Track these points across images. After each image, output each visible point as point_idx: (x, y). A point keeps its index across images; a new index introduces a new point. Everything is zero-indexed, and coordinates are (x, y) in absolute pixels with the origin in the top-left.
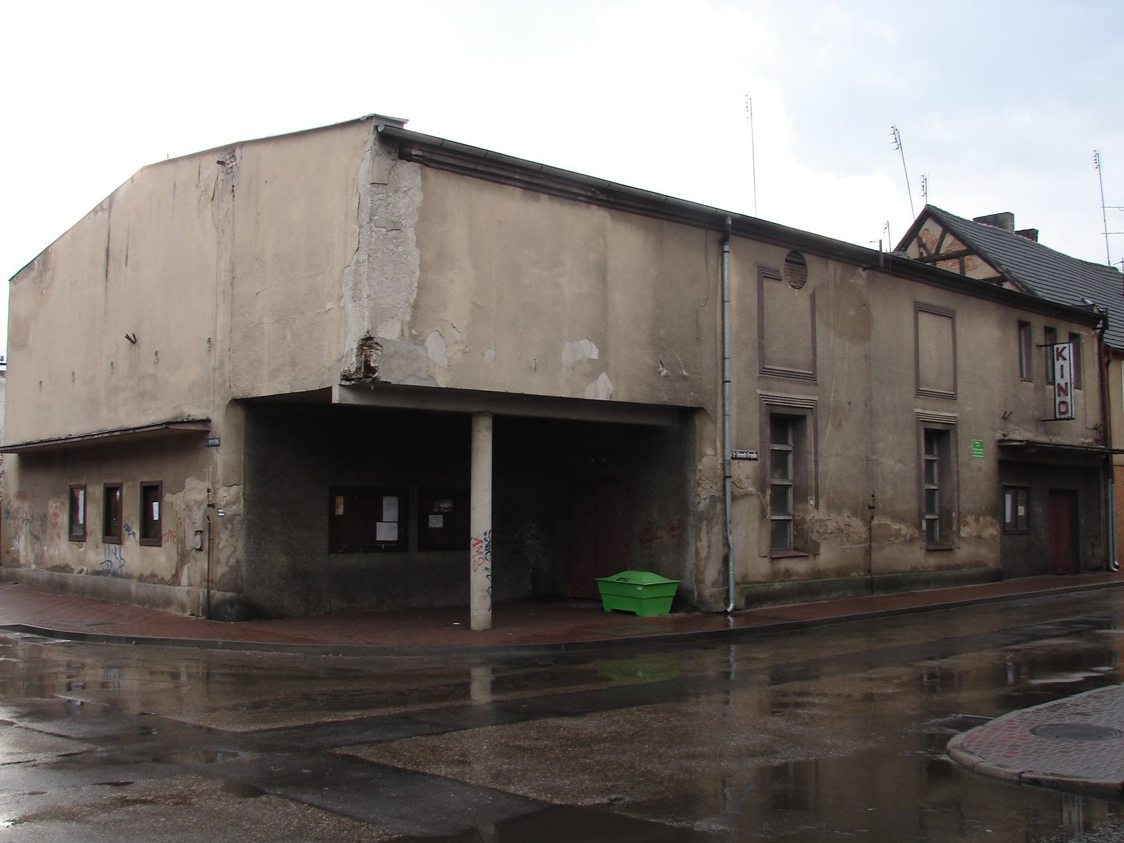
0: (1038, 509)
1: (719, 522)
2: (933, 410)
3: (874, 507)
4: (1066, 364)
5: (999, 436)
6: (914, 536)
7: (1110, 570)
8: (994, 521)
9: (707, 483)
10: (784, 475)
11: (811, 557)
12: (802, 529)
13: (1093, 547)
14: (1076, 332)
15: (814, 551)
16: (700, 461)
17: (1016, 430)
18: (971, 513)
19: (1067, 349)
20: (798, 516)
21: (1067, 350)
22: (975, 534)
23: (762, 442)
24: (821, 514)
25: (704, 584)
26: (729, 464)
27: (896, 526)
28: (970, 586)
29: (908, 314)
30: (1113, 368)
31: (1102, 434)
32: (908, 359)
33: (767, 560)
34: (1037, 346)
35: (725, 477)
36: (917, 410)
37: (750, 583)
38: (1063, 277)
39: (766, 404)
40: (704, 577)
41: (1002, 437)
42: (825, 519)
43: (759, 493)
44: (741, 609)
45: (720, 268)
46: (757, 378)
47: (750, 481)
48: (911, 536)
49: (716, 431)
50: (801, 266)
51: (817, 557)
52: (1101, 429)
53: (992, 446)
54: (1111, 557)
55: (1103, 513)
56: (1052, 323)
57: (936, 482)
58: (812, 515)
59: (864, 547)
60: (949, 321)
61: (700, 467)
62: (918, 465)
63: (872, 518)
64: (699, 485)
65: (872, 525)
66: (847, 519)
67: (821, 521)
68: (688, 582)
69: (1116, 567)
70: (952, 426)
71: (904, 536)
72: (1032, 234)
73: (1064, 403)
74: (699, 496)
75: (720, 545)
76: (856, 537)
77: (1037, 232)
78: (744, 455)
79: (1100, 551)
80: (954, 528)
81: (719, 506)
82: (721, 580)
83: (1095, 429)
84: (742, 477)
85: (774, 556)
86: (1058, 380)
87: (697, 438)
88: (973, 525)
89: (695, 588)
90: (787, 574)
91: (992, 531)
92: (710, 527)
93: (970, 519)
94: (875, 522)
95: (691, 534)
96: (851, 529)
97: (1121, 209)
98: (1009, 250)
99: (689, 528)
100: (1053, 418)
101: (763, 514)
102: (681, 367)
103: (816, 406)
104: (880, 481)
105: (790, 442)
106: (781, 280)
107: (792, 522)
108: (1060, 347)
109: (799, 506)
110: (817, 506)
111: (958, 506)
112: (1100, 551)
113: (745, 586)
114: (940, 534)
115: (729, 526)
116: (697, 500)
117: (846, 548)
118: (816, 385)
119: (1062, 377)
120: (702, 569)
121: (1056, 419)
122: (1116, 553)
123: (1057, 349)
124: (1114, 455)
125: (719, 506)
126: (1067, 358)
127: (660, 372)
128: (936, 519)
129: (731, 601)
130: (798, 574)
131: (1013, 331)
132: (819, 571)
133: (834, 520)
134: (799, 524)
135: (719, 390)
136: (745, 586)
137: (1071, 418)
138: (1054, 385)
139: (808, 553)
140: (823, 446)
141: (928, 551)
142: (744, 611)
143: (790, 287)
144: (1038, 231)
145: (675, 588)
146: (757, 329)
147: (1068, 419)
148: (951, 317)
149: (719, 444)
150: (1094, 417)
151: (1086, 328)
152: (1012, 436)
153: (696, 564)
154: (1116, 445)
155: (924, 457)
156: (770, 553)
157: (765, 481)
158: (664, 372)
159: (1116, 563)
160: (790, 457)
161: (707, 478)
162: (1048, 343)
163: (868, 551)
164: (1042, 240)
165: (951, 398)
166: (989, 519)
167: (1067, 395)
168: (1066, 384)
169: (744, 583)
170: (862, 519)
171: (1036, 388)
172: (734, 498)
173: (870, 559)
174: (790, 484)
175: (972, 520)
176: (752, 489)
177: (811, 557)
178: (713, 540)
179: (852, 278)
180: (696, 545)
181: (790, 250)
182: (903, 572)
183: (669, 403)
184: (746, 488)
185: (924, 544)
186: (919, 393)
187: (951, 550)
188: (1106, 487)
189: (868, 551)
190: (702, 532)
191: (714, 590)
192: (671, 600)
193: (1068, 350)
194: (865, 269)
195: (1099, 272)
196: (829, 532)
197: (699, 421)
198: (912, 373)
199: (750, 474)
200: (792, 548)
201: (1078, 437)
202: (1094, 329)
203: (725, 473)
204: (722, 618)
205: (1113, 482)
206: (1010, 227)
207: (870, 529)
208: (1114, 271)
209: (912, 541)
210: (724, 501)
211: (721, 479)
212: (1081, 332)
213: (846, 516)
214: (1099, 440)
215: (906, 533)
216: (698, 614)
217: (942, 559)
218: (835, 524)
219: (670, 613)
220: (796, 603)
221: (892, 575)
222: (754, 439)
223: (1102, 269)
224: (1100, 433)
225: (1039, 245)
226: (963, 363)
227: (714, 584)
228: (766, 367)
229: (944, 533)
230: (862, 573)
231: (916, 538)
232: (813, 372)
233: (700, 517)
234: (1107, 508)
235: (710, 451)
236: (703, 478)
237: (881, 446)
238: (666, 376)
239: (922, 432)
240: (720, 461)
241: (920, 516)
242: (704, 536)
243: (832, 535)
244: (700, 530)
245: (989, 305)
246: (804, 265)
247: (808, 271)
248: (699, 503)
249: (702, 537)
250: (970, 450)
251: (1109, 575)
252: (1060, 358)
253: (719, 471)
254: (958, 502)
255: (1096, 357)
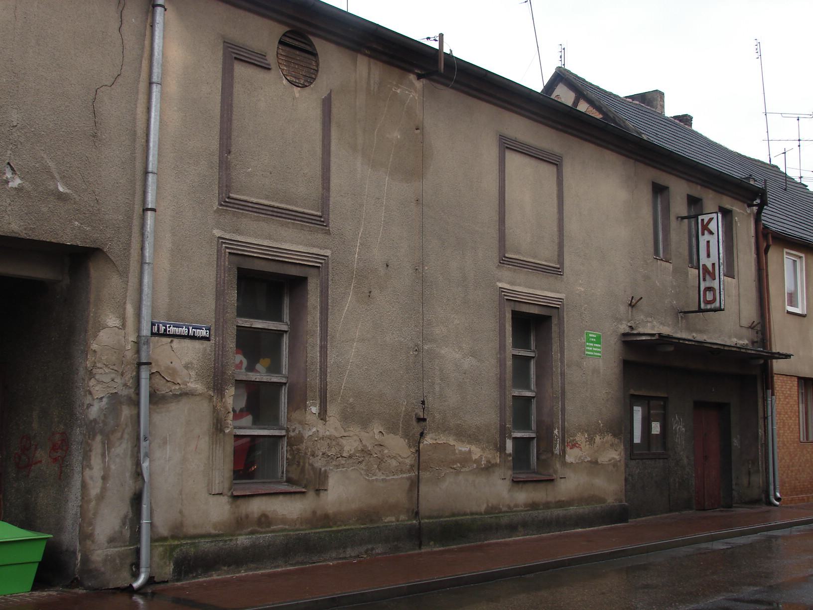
0: (679, 427)
1: (126, 436)
2: (526, 287)
3: (424, 420)
4: (713, 240)
5: (624, 328)
6: (493, 462)
7: (770, 504)
8: (617, 441)
9: (106, 373)
10: (275, 368)
11: (311, 495)
12: (298, 450)
13: (749, 474)
14: (728, 206)
15: (319, 484)
16: (95, 336)
17: (648, 322)
18: (581, 429)
19: (715, 220)
20: (294, 430)
21: (715, 220)
22: (589, 459)
23: (220, 310)
24: (333, 426)
25: (93, 542)
26: (147, 343)
27: (464, 448)
28: (580, 530)
29: (489, 152)
30: (773, 255)
31: (760, 334)
32: (489, 213)
33: (224, 500)
34: (678, 218)
35: (140, 364)
36: (500, 285)
37: (186, 537)
38: (718, 161)
39: (229, 253)
40: (93, 529)
41: (628, 330)
42: (337, 435)
43: (211, 393)
44: (167, 582)
45: (148, 33)
46: (215, 212)
47: (193, 373)
48: (489, 462)
49: (126, 290)
50: (310, 57)
51: (322, 494)
52: (759, 328)
53: (614, 343)
54: (772, 487)
55: (761, 432)
56: (697, 191)
57: (533, 387)
58: (314, 430)
59: (409, 478)
60: (554, 169)
61: (94, 346)
62: (502, 363)
63: (422, 434)
64: (91, 374)
65: (421, 445)
66: (377, 437)
67: (330, 438)
68: (70, 538)
69: (778, 499)
70: (555, 311)
71: (477, 461)
72: (686, 120)
73: (709, 289)
74: (90, 393)
75: (128, 475)
76: (394, 463)
77: (691, 118)
78: (183, 331)
79: (758, 480)
80: (557, 450)
81: (126, 412)
82: (127, 533)
83: (751, 327)
84: (178, 365)
85: (235, 493)
86: (704, 260)
87: (92, 300)
88: (585, 446)
89: (78, 548)
90: (264, 520)
91: (613, 454)
92: (108, 445)
93: (581, 438)
94: (428, 440)
95: (76, 458)
96: (386, 451)
97: (784, 115)
98: (654, 125)
99: (74, 447)
100: (697, 309)
101: (218, 426)
102: (53, 178)
103: (327, 264)
104: (438, 381)
105: (286, 317)
106: (269, 69)
107: (536, 439)
108: (706, 218)
109: (296, 415)
110: (323, 415)
111: (563, 421)
112: (758, 480)
113: (176, 542)
114: (538, 458)
115: (143, 444)
116: (88, 400)
117: (376, 480)
118: (328, 233)
119: (708, 256)
120: (91, 515)
121: (700, 310)
122: (777, 483)
123: (703, 220)
124: (774, 361)
125: (126, 412)
126: (715, 231)
127: (7, 182)
128: (534, 438)
129: (143, 570)
130: (284, 521)
131: (646, 195)
132: (326, 516)
133: (355, 438)
134: (294, 442)
135: (136, 222)
136: (176, 542)
137: (720, 309)
138: (699, 269)
139: (305, 487)
140: (336, 324)
141: (516, 482)
142: (170, 584)
143: (285, 82)
144: (692, 118)
145: (43, 545)
146: (217, 137)
147: (715, 310)
148: (557, 165)
149: (130, 310)
150: (749, 313)
151: (740, 204)
152: (641, 330)
153: (81, 506)
154: (777, 348)
155: (510, 351)
156: (230, 489)
157: (223, 373)
158: (16, 182)
159: (778, 495)
160: (285, 339)
161: (106, 366)
162: (693, 213)
163: (415, 484)
164: (696, 126)
165: (556, 271)
166: (609, 438)
167: (715, 279)
168: (713, 264)
169: (174, 537)
170: (406, 435)
171: (675, 271)
172: (156, 399)
173: (418, 495)
174: (284, 380)
175: (583, 440)
176: (196, 386)
177: (311, 495)
178: (113, 467)
179: (399, 87)
180: (83, 476)
181: (287, 29)
182: (472, 514)
183: (23, 235)
184: (185, 383)
185: (509, 473)
186: (504, 261)
187: (552, 480)
188: (765, 400)
189: (415, 484)
190: (93, 454)
191: (112, 551)
192: (35, 567)
193: (716, 223)
194: (419, 77)
195: (759, 167)
196: (344, 455)
197: (96, 271)
198: (494, 232)
199: (195, 362)
200: (285, 479)
201: (730, 337)
202: (750, 205)
203: (139, 357)
204: (122, 599)
205: (773, 394)
206: (659, 107)
207: (418, 451)
208: (775, 169)
209: (489, 468)
210: (136, 403)
211: (134, 367)
212: (734, 208)
213: (376, 431)
214: (757, 342)
215: (481, 457)
216: (81, 591)
217: (539, 494)
218: (358, 443)
219: (35, 588)
220: (278, 566)
221: (454, 519)
222: (207, 308)
223: (763, 165)
224: (757, 333)
225: (693, 131)
226: (572, 226)
227: (112, 540)
228: (232, 195)
229: (543, 457)
230: (402, 517)
231: (495, 465)
232: (322, 212)
233: (92, 428)
234: (766, 426)
235: (112, 321)
236: (99, 365)
237: (438, 331)
238: (19, 189)
239: (509, 316)
240: (132, 338)
241: (503, 433)
242: (96, 461)
243: (350, 461)
244: (90, 450)
245: (611, 158)
246: (314, 54)
247: (321, 65)
248: (90, 405)
249: (93, 462)
250: (583, 345)
251: (768, 512)
252: (706, 232)
253: (130, 355)
254: (563, 414)
255: (753, 240)
